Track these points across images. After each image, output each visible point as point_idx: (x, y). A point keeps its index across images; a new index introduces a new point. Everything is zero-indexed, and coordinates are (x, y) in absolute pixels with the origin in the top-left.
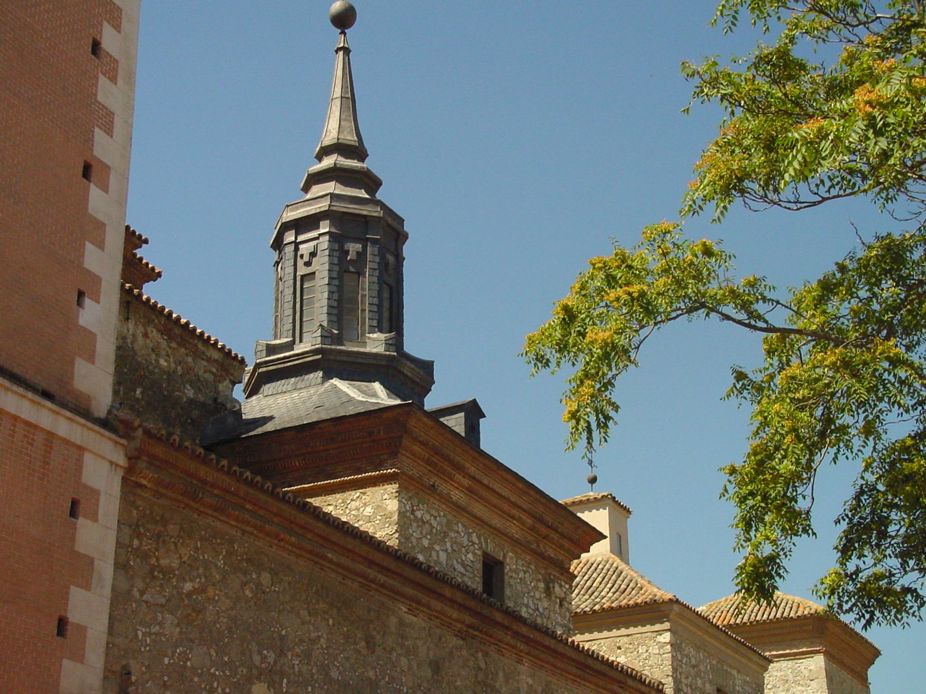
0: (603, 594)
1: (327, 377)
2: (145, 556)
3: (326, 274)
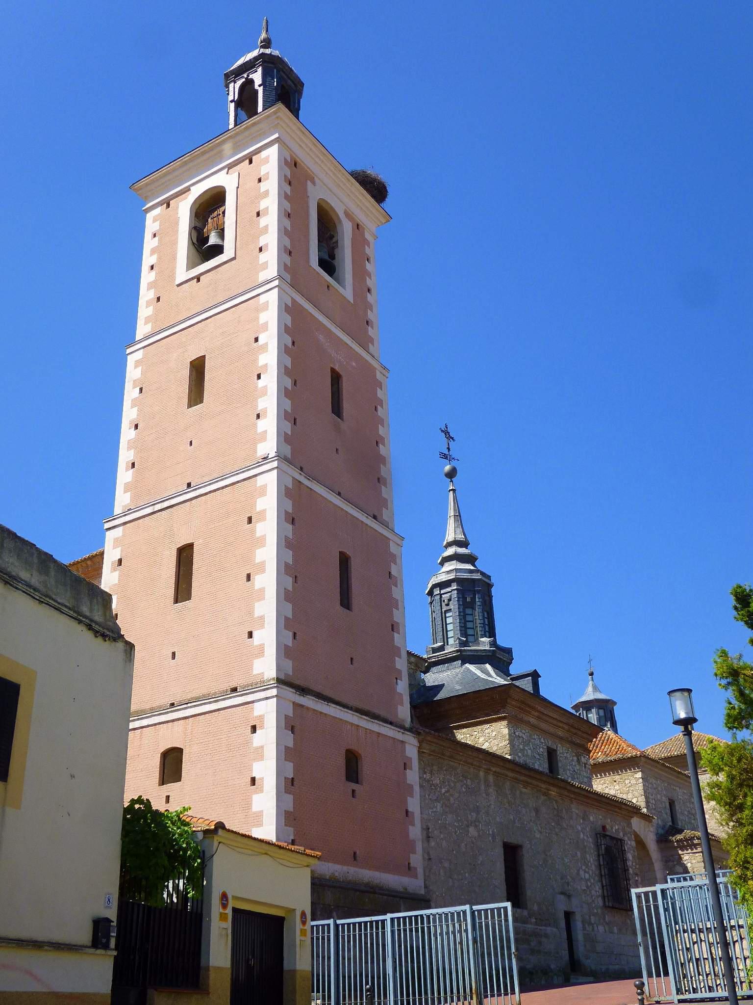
1: (463, 663)
2: (428, 781)
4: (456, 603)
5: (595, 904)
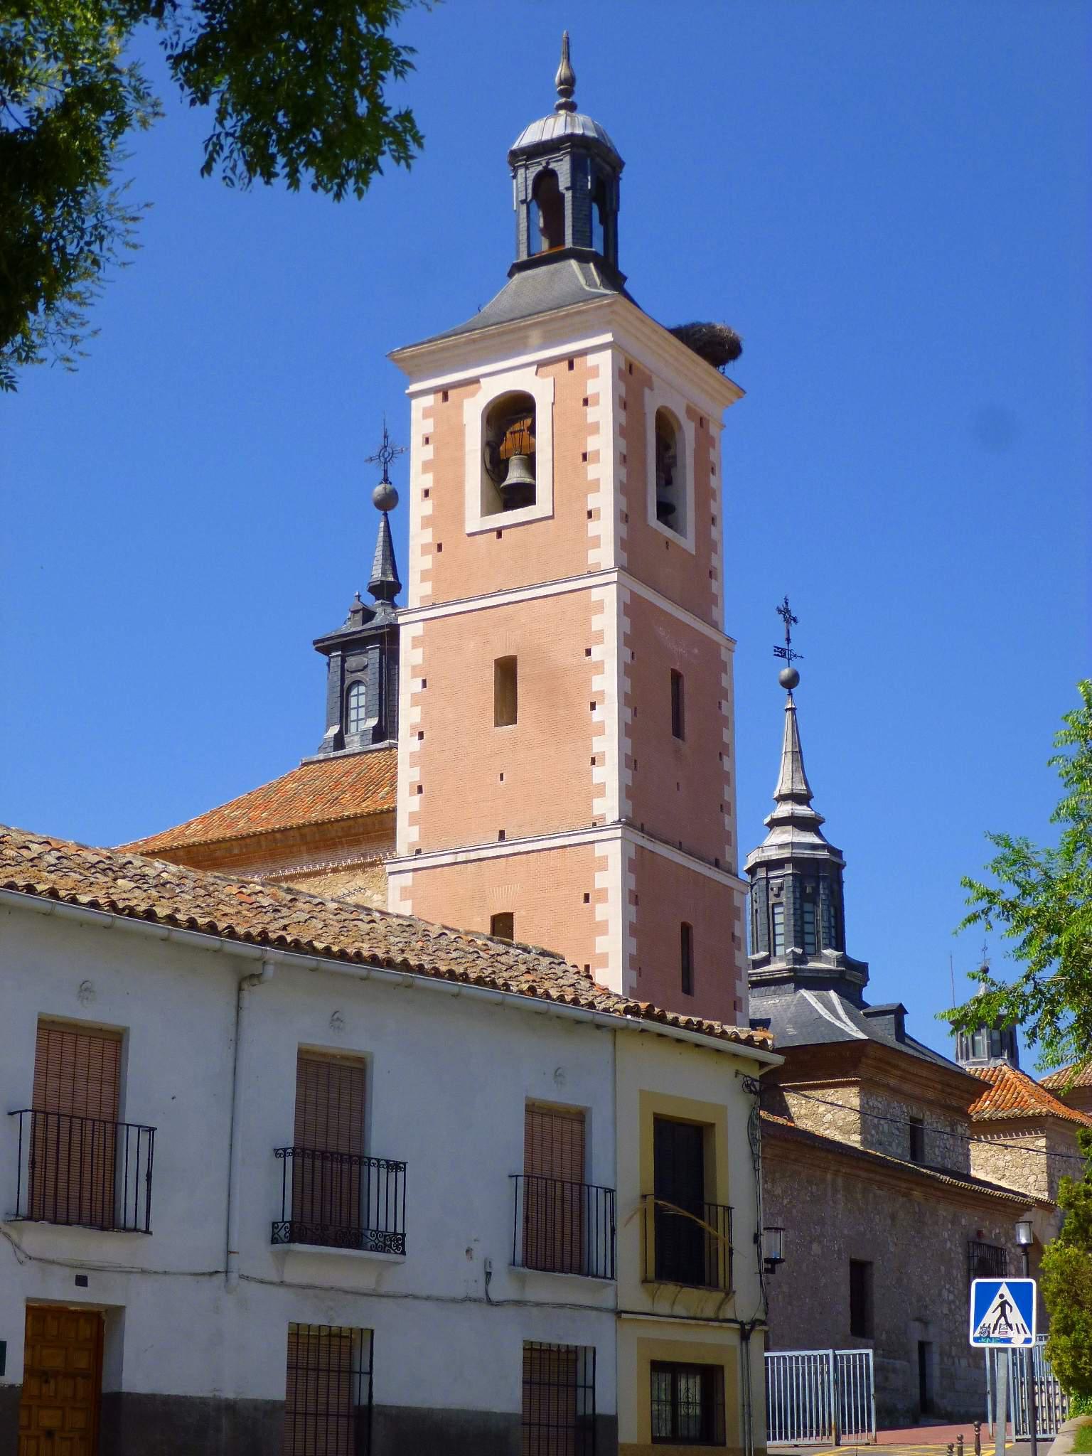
1: (797, 988)
4: (791, 895)
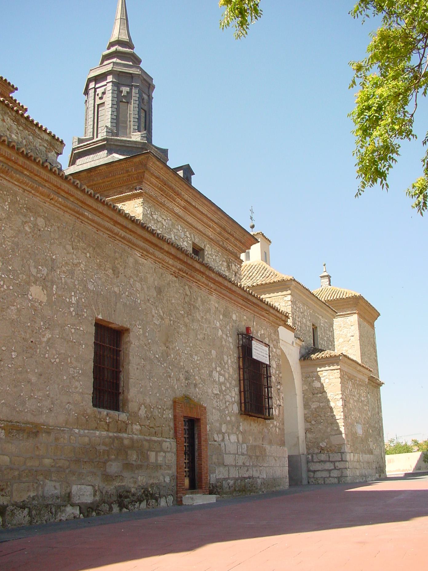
0: (258, 278)
3: (110, 102)
5: (228, 410)
